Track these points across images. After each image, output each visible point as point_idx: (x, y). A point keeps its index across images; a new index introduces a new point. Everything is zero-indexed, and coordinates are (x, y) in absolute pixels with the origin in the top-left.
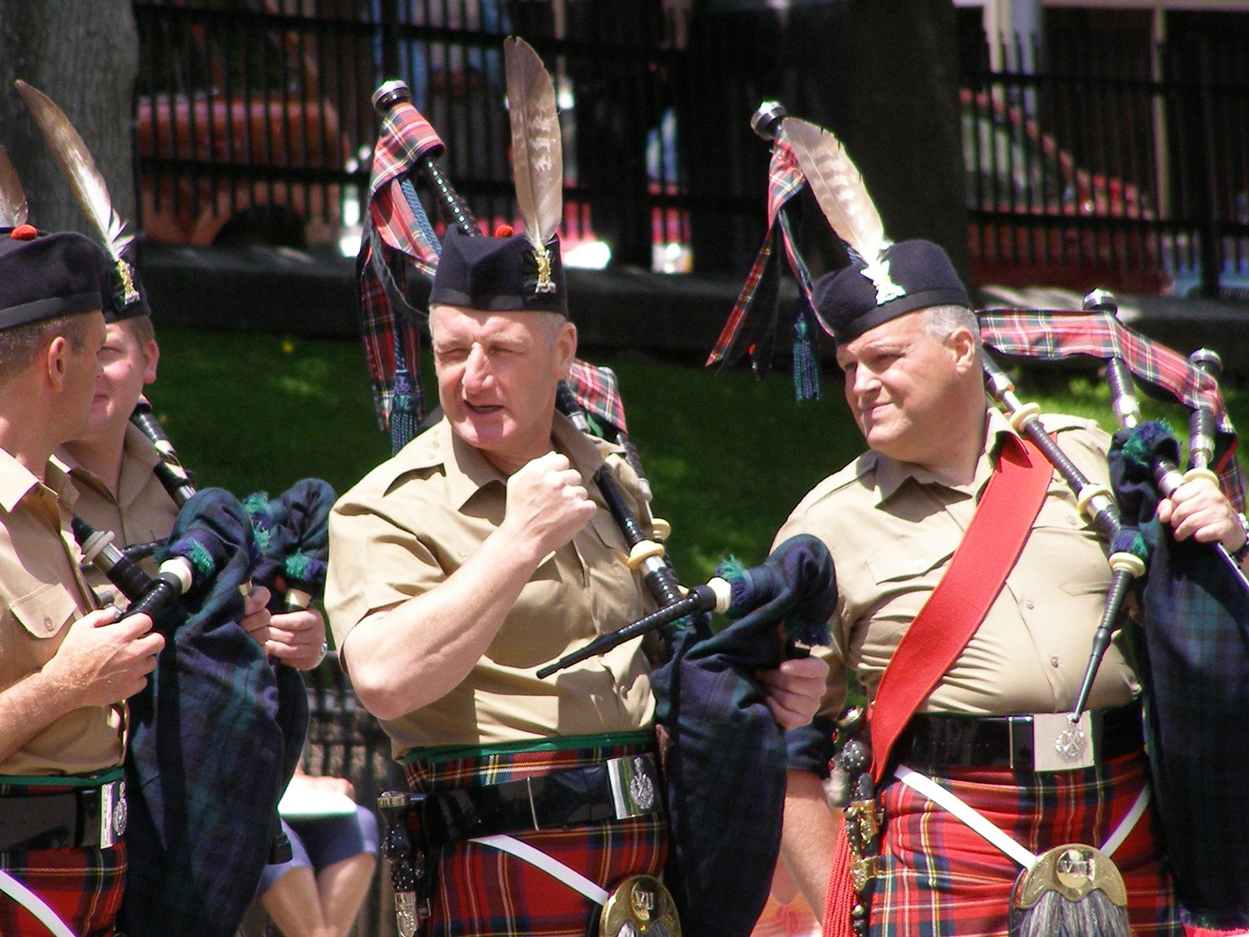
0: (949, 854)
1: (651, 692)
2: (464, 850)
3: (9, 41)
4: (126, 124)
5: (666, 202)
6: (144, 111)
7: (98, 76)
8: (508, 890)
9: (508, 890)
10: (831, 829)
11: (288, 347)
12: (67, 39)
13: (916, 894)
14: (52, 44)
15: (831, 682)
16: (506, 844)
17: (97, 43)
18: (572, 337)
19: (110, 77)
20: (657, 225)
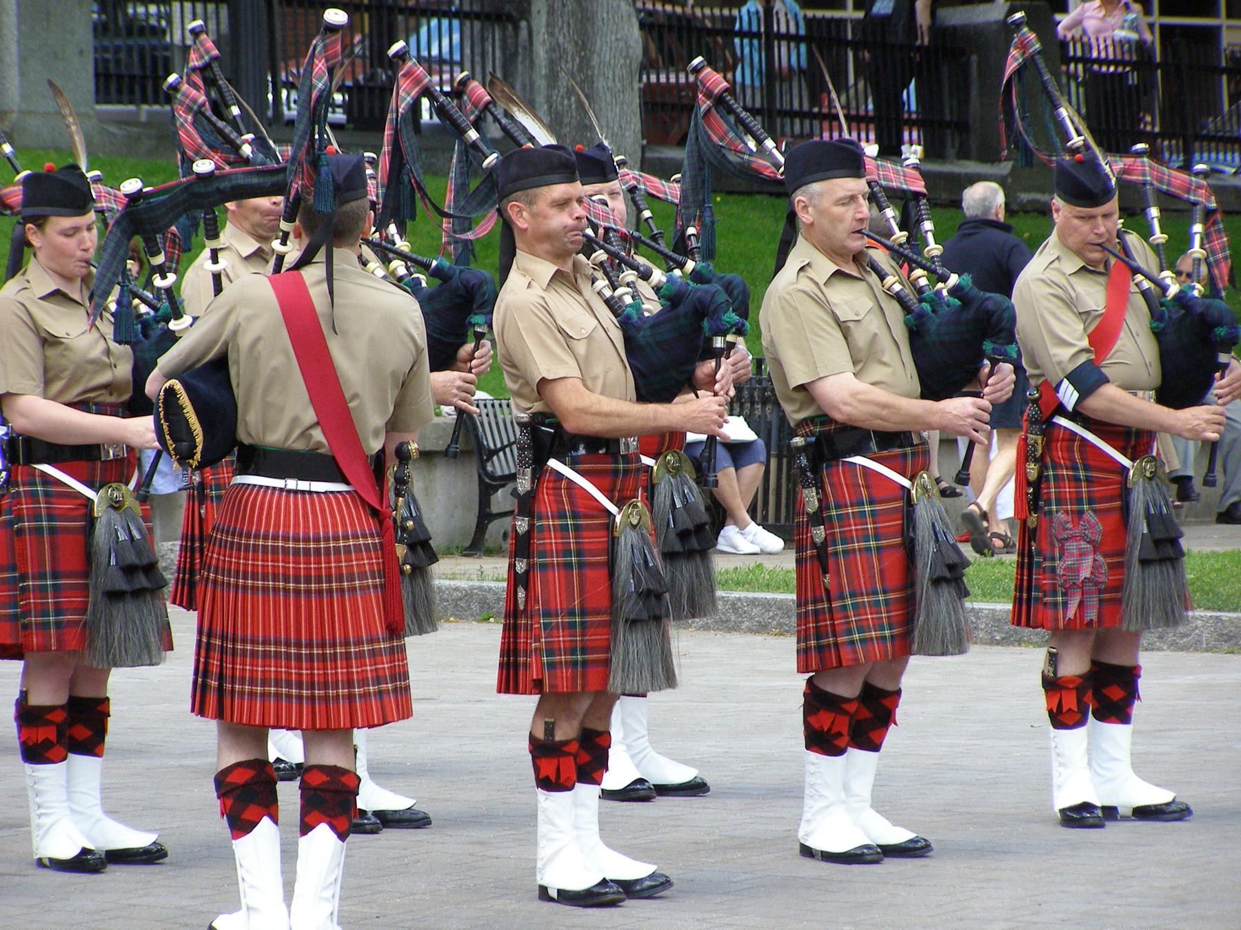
0: (1090, 462)
1: (1014, 478)
2: (838, 465)
3: (576, 43)
4: (636, 86)
5: (911, 124)
6: (645, 78)
7: (622, 61)
8: (764, 69)
9: (764, 69)
10: (588, 19)
11: (718, 199)
12: (607, 42)
13: (1073, 484)
14: (598, 46)
15: (1015, 373)
16: (858, 460)
17: (621, 44)
18: (562, 361)
19: (628, 62)
20: (906, 134)
